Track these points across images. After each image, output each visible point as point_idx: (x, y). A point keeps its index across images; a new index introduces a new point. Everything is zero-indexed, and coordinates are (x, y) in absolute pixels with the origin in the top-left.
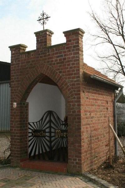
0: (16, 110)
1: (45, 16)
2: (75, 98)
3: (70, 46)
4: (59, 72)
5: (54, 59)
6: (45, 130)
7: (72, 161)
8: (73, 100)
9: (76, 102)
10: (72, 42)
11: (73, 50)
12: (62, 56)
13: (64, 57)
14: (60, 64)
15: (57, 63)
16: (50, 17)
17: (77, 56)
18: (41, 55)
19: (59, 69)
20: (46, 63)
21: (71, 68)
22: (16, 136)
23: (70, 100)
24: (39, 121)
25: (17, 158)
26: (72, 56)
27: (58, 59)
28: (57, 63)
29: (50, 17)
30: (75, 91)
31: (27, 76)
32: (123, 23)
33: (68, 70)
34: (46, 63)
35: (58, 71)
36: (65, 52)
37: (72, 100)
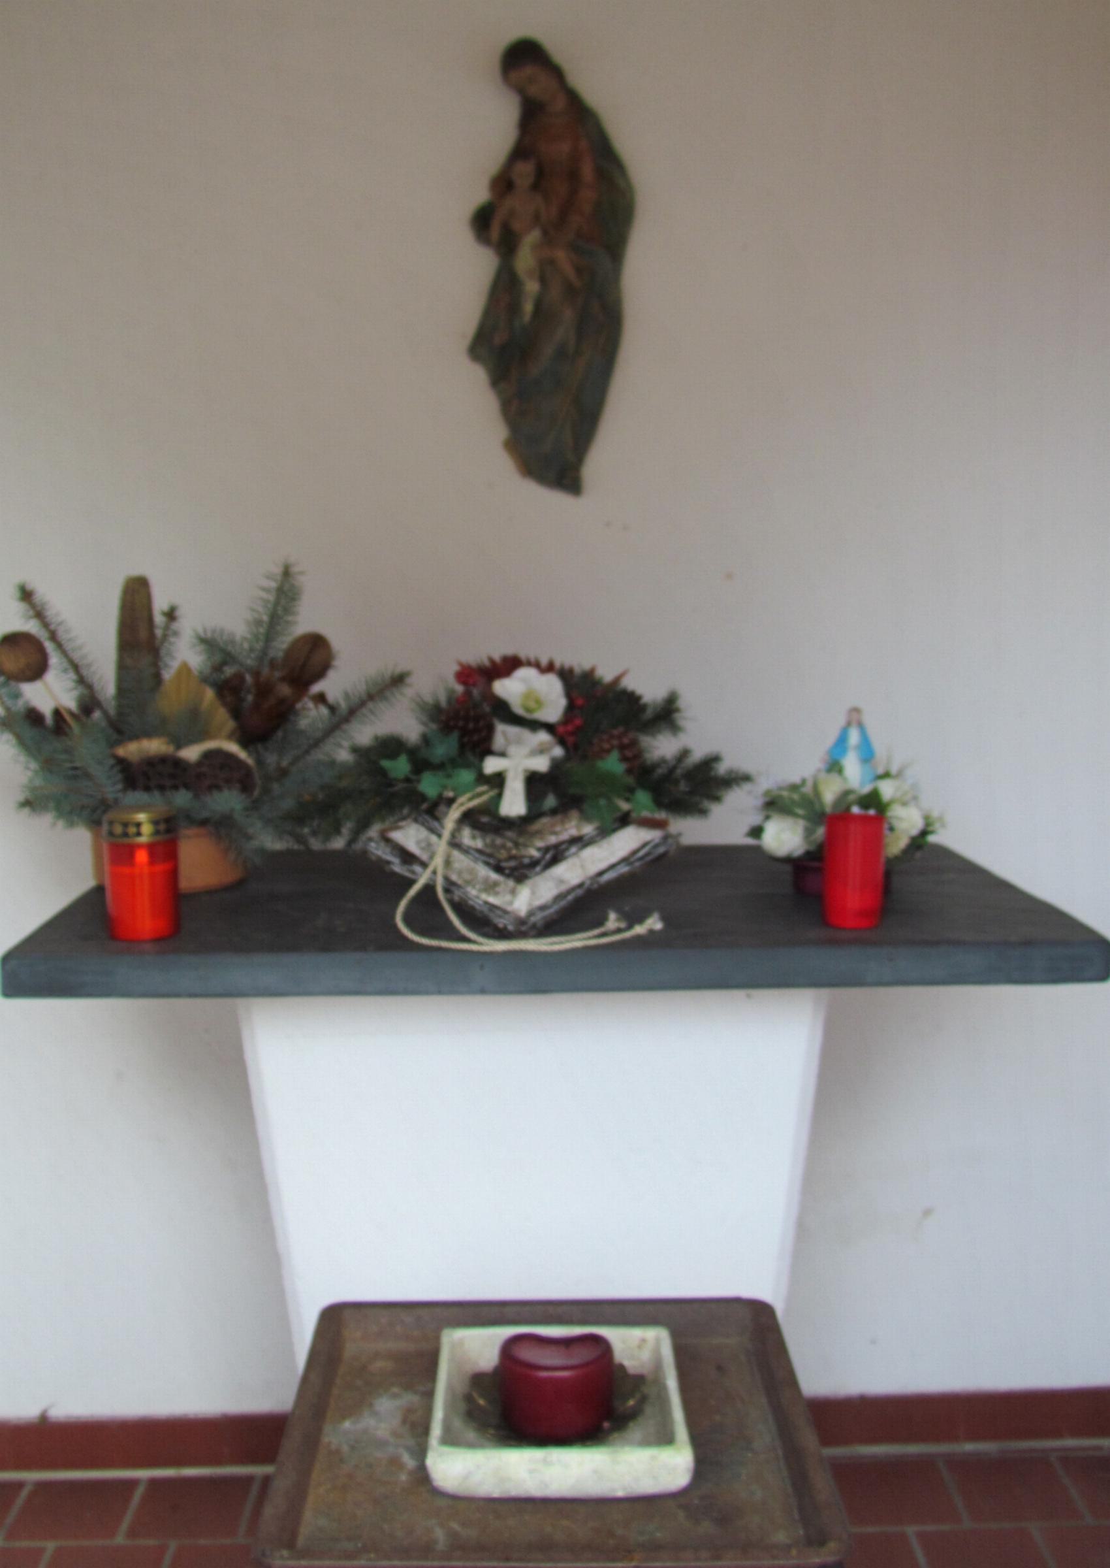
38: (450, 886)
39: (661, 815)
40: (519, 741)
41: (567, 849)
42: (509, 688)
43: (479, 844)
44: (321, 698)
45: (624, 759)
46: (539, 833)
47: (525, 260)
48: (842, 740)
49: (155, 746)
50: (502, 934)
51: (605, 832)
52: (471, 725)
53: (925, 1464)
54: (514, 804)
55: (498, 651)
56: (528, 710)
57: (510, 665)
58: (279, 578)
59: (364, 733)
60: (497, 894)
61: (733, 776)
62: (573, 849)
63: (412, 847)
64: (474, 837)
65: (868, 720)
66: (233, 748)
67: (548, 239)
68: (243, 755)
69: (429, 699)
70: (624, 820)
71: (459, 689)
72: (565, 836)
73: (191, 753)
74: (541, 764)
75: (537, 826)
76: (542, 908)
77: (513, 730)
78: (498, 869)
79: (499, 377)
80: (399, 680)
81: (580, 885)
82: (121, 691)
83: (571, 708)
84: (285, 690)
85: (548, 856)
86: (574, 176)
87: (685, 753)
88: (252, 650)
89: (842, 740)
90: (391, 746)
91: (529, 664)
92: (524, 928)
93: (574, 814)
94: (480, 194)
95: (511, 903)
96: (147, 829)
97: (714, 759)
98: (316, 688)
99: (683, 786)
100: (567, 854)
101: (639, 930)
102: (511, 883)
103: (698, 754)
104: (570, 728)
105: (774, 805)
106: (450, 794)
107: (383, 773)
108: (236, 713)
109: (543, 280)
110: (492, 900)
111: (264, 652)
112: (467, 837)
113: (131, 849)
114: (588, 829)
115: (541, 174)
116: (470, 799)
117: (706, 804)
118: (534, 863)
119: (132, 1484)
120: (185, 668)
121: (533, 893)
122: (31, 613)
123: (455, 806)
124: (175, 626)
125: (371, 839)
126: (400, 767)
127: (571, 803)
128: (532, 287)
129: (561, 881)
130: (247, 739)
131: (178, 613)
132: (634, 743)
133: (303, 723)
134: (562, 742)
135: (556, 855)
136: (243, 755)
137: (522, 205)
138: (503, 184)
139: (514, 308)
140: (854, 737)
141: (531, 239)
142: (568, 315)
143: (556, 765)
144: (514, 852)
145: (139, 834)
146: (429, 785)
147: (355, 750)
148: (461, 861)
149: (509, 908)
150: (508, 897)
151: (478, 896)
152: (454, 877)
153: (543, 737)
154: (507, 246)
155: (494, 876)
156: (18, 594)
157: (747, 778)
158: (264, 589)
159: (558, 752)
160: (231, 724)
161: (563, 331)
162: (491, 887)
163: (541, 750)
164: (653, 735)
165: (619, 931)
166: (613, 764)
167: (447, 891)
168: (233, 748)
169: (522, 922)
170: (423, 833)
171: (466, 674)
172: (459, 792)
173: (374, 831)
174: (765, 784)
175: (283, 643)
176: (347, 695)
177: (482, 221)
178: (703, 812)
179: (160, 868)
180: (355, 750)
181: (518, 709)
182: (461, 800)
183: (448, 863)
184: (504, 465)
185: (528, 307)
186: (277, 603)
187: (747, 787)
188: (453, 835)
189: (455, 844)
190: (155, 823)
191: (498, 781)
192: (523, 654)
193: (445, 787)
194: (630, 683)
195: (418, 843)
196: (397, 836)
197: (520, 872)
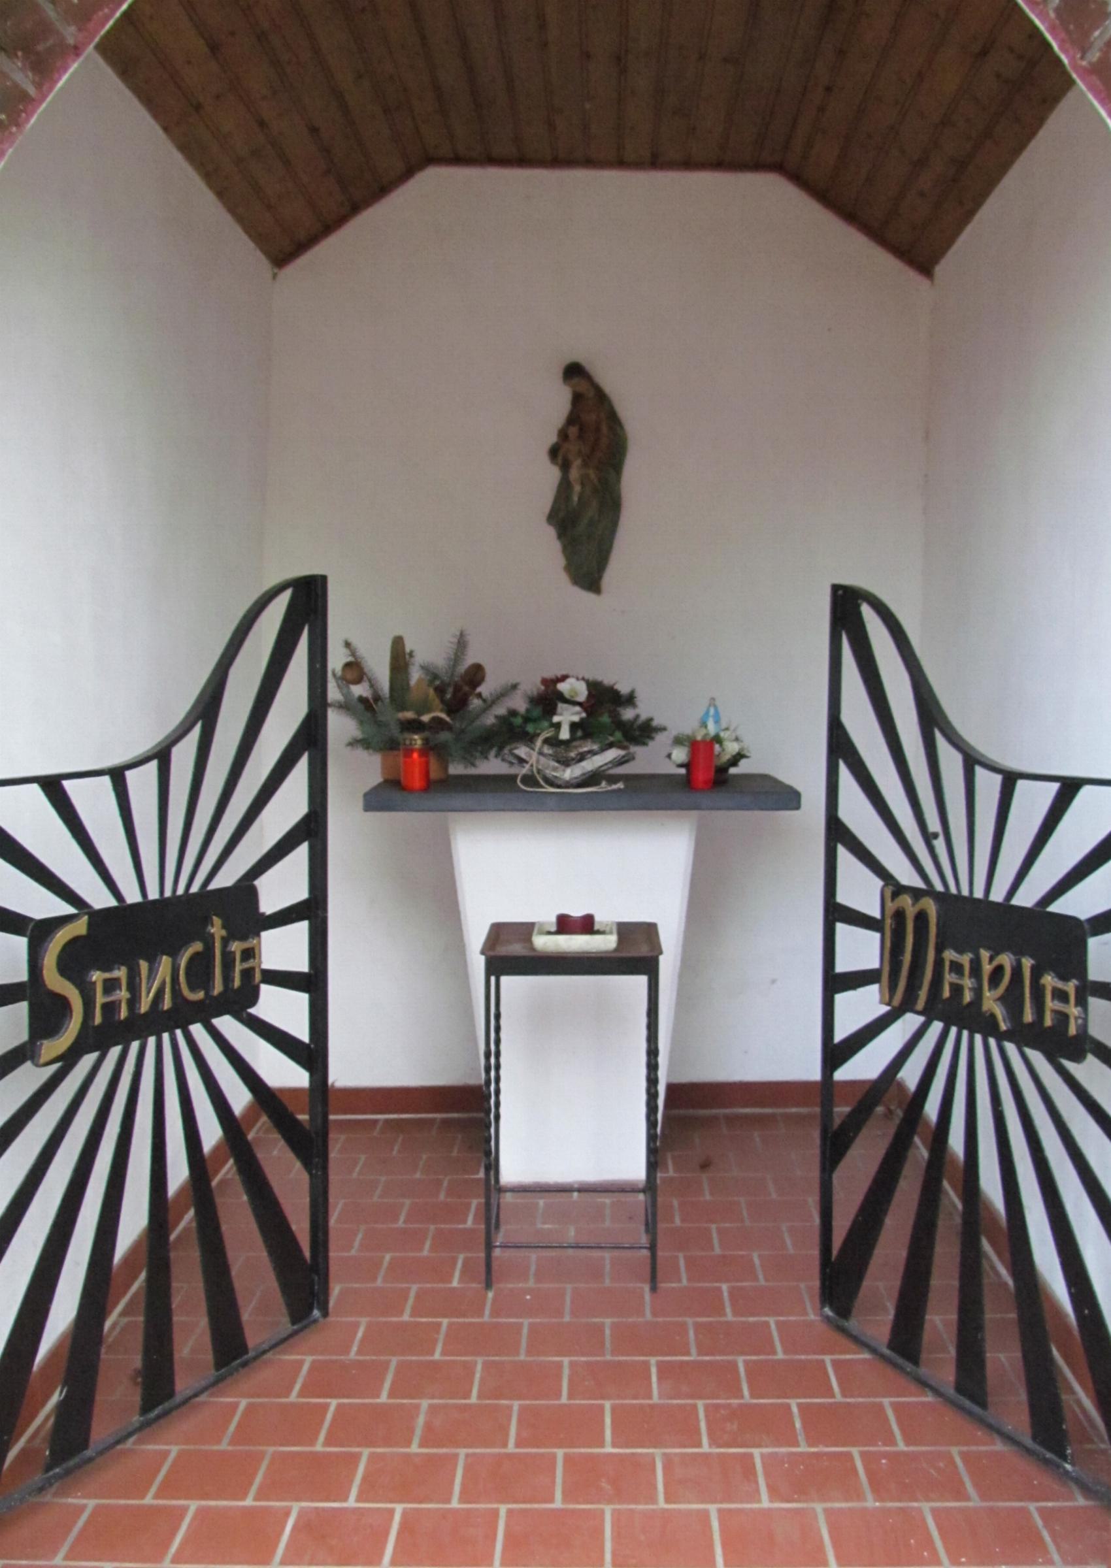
6: (246, 889)
24: (162, 756)
38: (539, 771)
39: (626, 743)
40: (567, 710)
41: (587, 755)
42: (562, 687)
43: (550, 752)
44: (479, 695)
45: (610, 717)
46: (576, 747)
47: (574, 474)
48: (707, 713)
49: (409, 715)
50: (559, 787)
51: (603, 750)
52: (547, 702)
53: (773, 1116)
54: (565, 734)
55: (559, 674)
56: (572, 697)
57: (564, 678)
58: (458, 637)
59: (501, 710)
60: (557, 772)
61: (659, 727)
62: (589, 756)
63: (523, 756)
64: (548, 749)
65: (718, 703)
66: (443, 716)
67: (585, 464)
68: (448, 719)
69: (529, 693)
70: (611, 745)
71: (543, 688)
72: (585, 749)
73: (426, 718)
74: (576, 719)
75: (574, 744)
76: (576, 778)
77: (565, 706)
78: (558, 762)
79: (562, 534)
80: (515, 687)
81: (592, 771)
82: (392, 688)
83: (590, 695)
84: (466, 688)
85: (579, 757)
86: (598, 430)
87: (638, 716)
88: (447, 673)
89: (707, 713)
90: (513, 713)
91: (573, 677)
92: (568, 785)
93: (589, 740)
94: (553, 438)
95: (563, 775)
96: (419, 742)
97: (651, 719)
98: (479, 690)
99: (637, 733)
100: (586, 757)
101: (614, 787)
102: (563, 767)
103: (644, 717)
104: (588, 705)
105: (678, 741)
106: (538, 731)
107: (511, 724)
108: (443, 701)
109: (583, 484)
110: (555, 774)
111: (452, 675)
112: (547, 750)
113: (412, 751)
114: (595, 747)
115: (581, 430)
116: (547, 733)
117: (647, 740)
118: (573, 759)
119: (376, 1122)
121: (572, 771)
122: (350, 653)
123: (541, 736)
124: (412, 660)
125: (505, 754)
126: (518, 721)
127: (588, 735)
128: (577, 488)
129: (583, 767)
130: (450, 712)
131: (414, 654)
132: (615, 710)
133: (471, 707)
134: (585, 710)
135: (582, 758)
136: (448, 719)
137: (572, 447)
138: (563, 434)
139: (568, 498)
140: (712, 711)
141: (577, 463)
142: (595, 504)
143: (582, 720)
144: (564, 755)
145: (416, 744)
146: (530, 728)
147: (496, 717)
148: (542, 759)
149: (562, 777)
150: (562, 773)
151: (550, 773)
152: (540, 767)
153: (578, 709)
154: (565, 467)
155: (556, 764)
156: (343, 644)
157: (664, 729)
158: (451, 643)
159: (584, 715)
160: (441, 706)
161: (591, 512)
162: (555, 769)
163: (577, 713)
164: (625, 709)
165: (605, 787)
166: (605, 719)
167: (539, 773)
168: (443, 716)
169: (567, 782)
170: (527, 749)
171: (545, 681)
172: (543, 730)
173: (506, 751)
174: (673, 732)
175: (462, 668)
176: (491, 694)
177: (554, 452)
178: (645, 744)
179: (423, 759)
180: (496, 717)
181: (567, 695)
182: (543, 734)
183: (538, 761)
184: (564, 579)
185: (575, 498)
186: (457, 650)
187: (665, 734)
188: (540, 749)
189: (541, 753)
190: (423, 739)
191: (558, 726)
192: (571, 673)
193: (536, 729)
194: (618, 687)
195: (526, 754)
196: (517, 752)
197: (566, 763)
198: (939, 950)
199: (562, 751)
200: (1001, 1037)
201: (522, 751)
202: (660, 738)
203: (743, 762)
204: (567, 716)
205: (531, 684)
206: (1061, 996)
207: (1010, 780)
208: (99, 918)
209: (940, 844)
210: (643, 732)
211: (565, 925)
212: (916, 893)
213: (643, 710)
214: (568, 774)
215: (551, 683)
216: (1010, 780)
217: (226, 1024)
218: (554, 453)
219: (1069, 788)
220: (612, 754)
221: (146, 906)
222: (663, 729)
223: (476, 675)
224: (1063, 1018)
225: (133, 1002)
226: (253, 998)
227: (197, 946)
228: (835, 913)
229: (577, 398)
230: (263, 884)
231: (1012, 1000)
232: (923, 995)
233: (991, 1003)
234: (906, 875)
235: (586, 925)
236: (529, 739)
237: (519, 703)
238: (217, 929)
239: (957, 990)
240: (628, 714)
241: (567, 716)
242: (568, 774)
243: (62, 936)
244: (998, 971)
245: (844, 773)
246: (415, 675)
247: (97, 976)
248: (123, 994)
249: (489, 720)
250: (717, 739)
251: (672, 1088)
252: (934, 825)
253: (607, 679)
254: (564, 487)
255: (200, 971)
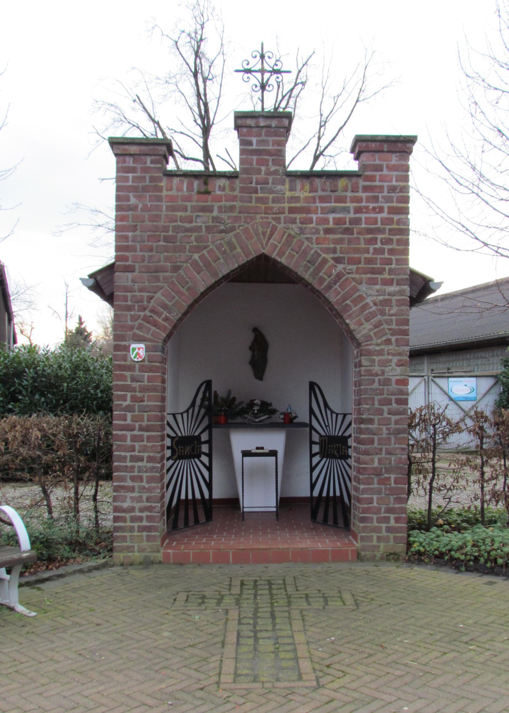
0: (143, 368)
1: (255, 64)
2: (388, 342)
3: (377, 183)
4: (333, 259)
5: (314, 217)
6: (199, 437)
7: (375, 524)
8: (382, 347)
9: (394, 355)
10: (385, 172)
11: (388, 200)
12: (346, 210)
13: (352, 215)
14: (340, 236)
15: (328, 231)
16: (237, 71)
17: (399, 219)
18: (260, 195)
19: (334, 251)
20: (282, 225)
21: (380, 251)
22: (141, 459)
23: (367, 347)
24: (187, 411)
25: (145, 534)
26: (385, 215)
27: (331, 217)
28: (328, 231)
29: (237, 71)
30: (389, 322)
31: (196, 256)
32: (323, 135)
33: (366, 255)
34: (282, 225)
35: (332, 255)
36: (359, 200)
37: (377, 348)
42: (255, 402)
47: (256, 353)
49: (219, 408)
54: (256, 412)
57: (255, 400)
59: (240, 407)
73: (223, 409)
90: (243, 408)
105: (282, 414)
120: (270, 169)
135: (260, 417)
154: (253, 352)
184: (253, 377)
191: (254, 410)
197: (257, 418)
198: (328, 445)
199: (256, 416)
200: (337, 458)
201: (246, 416)
202: (278, 413)
203: (297, 419)
204: (256, 408)
205: (247, 401)
206: (345, 449)
207: (337, 415)
208: (180, 437)
209: (328, 428)
210: (274, 412)
211: (258, 448)
212: (324, 436)
213: (274, 407)
214: (257, 420)
215: (252, 401)
216: (337, 415)
217: (196, 460)
218: (251, 348)
219: (345, 415)
220: (266, 416)
221: (185, 436)
222: (278, 411)
223: (234, 399)
224: (345, 452)
225: (184, 452)
226: (200, 456)
227: (193, 445)
228: (312, 443)
229: (256, 337)
230: (202, 436)
231: (338, 452)
232: (326, 454)
233: (336, 454)
234: (323, 434)
235: (262, 448)
236: (248, 413)
237: (244, 405)
238: (195, 442)
239: (331, 452)
240: (270, 408)
241: (256, 408)
242: (257, 420)
243: (176, 439)
244: (336, 447)
245: (313, 418)
246: (219, 400)
247: (180, 447)
248: (183, 451)
249: (237, 409)
250: (291, 413)
251: (281, 498)
252: (327, 424)
253: (265, 400)
254: (253, 356)
255: (193, 449)
